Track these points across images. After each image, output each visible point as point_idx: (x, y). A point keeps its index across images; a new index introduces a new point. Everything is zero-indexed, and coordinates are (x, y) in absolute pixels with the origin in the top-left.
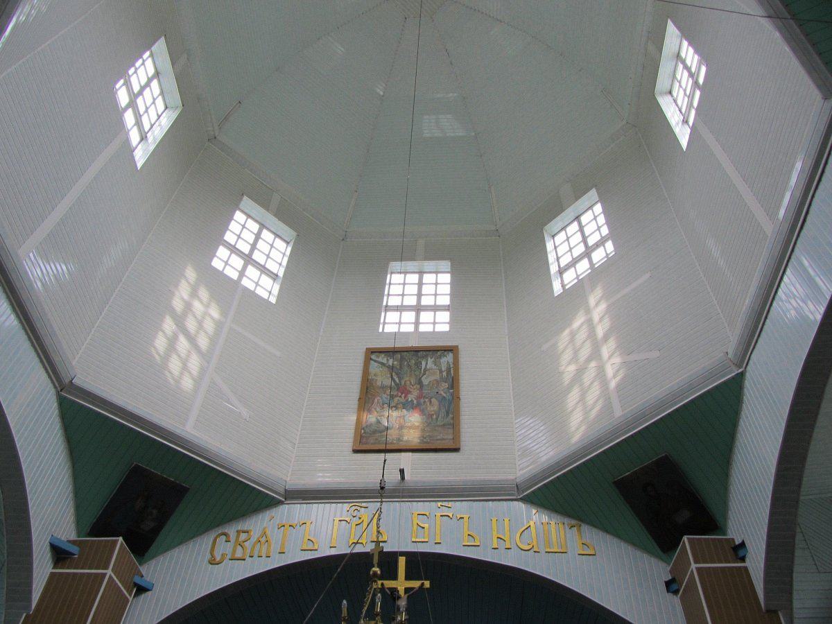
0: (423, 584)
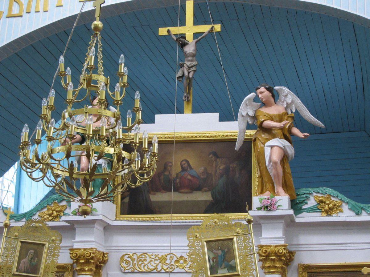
0: (212, 29)
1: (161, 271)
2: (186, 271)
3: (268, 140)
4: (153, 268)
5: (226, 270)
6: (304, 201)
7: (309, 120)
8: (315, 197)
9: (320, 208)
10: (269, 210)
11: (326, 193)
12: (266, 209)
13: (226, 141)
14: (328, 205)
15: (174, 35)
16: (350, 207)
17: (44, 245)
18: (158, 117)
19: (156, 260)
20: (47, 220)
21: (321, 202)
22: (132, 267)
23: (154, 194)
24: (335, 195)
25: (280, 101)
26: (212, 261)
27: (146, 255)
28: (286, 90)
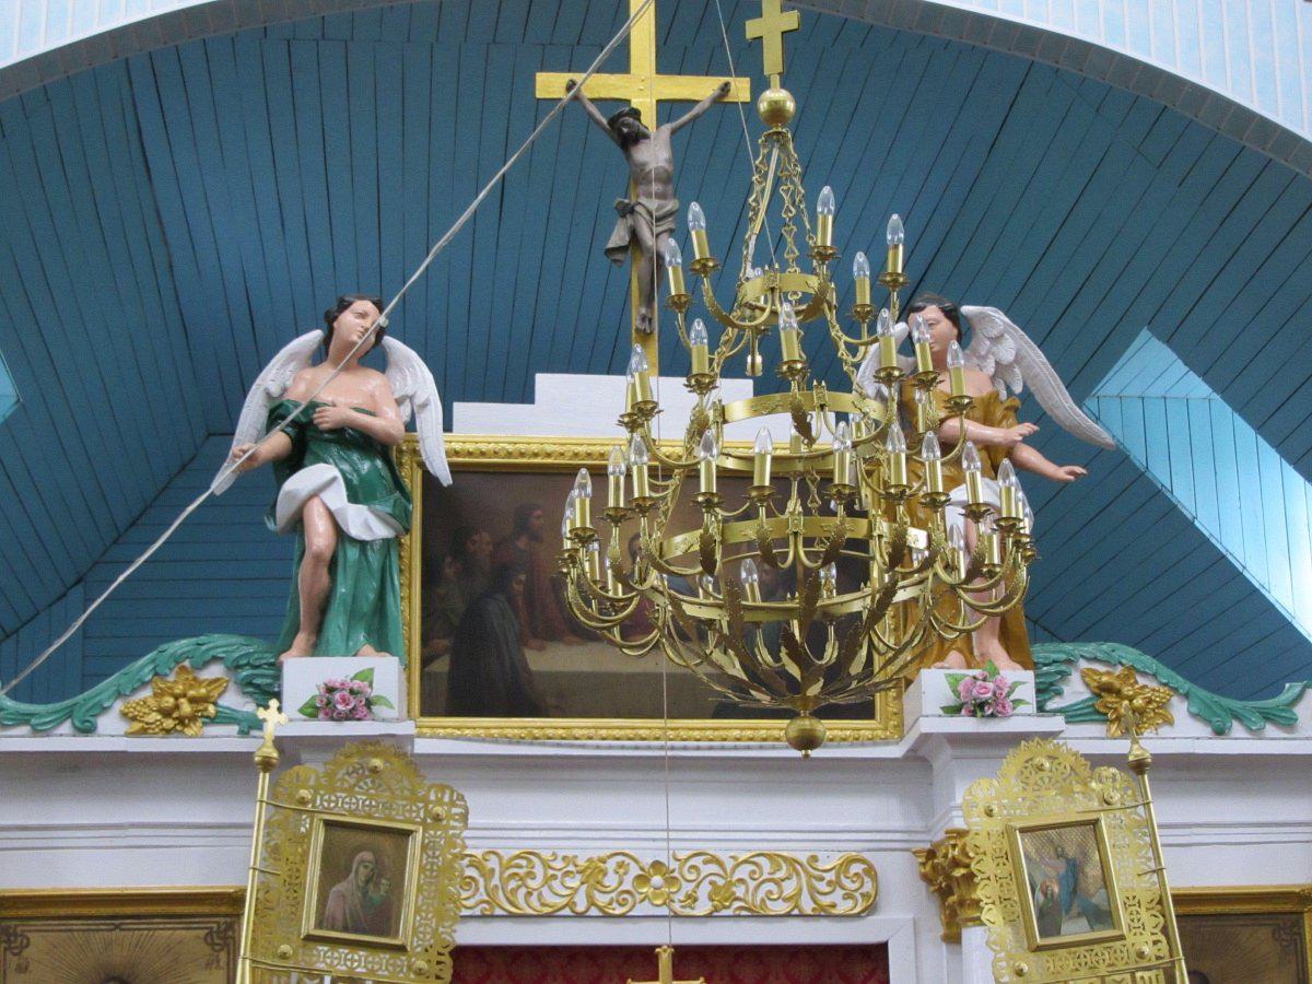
0: (725, 88)
1: (588, 914)
2: (675, 913)
4: (564, 901)
5: (1083, 922)
6: (1052, 684)
7: (1067, 423)
8: (1084, 674)
9: (1102, 710)
10: (988, 716)
11: (1120, 663)
12: (979, 714)
13: (497, 470)
14: (1131, 701)
16: (1194, 710)
17: (407, 834)
18: (542, 380)
19: (567, 873)
20: (157, 730)
21: (1108, 689)
22: (486, 898)
23: (541, 649)
24: (1148, 668)
26: (1043, 892)
27: (531, 857)
28: (999, 318)
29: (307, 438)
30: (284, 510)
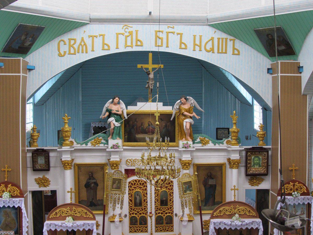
3: (185, 119)
8: (200, 138)
15: (144, 68)
18: (138, 103)
21: (202, 140)
23: (138, 135)
25: (188, 101)
28: (191, 98)
29: (111, 114)
30: (108, 123)
